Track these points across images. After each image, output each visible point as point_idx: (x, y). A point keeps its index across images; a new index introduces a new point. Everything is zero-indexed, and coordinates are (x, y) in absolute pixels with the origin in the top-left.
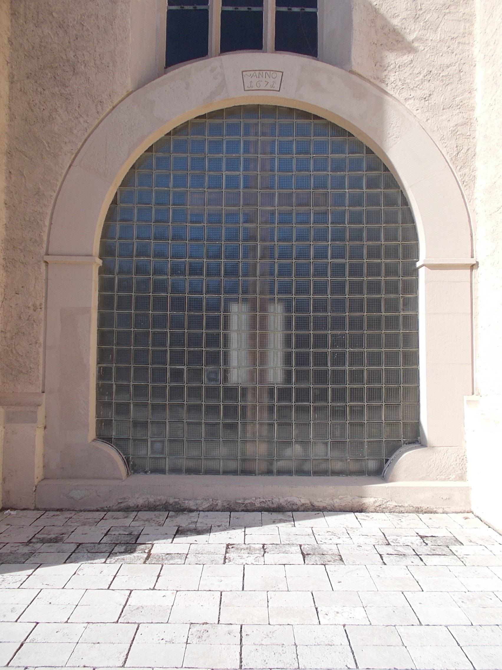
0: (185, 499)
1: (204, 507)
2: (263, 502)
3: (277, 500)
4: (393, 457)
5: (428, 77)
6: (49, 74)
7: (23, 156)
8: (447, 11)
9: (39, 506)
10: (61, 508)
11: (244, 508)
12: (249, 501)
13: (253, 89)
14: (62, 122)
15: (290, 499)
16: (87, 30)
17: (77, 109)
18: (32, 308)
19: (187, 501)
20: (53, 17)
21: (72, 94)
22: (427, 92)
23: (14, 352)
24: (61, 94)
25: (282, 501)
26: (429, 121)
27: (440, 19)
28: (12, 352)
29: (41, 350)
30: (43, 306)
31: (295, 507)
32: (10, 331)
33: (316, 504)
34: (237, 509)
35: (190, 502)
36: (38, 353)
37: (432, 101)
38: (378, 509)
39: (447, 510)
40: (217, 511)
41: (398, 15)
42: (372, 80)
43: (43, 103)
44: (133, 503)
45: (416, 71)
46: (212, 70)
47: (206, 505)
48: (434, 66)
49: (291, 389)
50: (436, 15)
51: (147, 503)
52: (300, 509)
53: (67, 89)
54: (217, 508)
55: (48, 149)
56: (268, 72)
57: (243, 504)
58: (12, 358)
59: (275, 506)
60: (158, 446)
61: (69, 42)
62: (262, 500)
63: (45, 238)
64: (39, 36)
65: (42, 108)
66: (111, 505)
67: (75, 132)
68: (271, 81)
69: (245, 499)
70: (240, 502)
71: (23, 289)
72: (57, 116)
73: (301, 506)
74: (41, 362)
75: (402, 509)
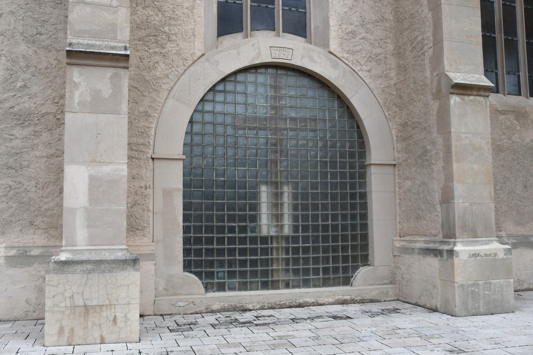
0: (246, 304)
1: (258, 307)
2: (291, 302)
3: (298, 301)
4: (356, 274)
5: (370, 59)
6: (153, 40)
7: (137, 90)
8: (378, 24)
9: (157, 313)
10: (171, 313)
11: (280, 307)
12: (283, 303)
13: (277, 58)
14: (161, 70)
15: (305, 300)
16: (177, 15)
17: (171, 63)
18: (144, 188)
19: (247, 305)
20: (155, 5)
21: (168, 53)
22: (369, 68)
23: (134, 216)
24: (161, 53)
25: (301, 301)
26: (51, 30)
27: (374, 28)
28: (132, 217)
29: (151, 214)
30: (151, 187)
31: (308, 304)
32: (130, 203)
33: (319, 302)
34: (276, 308)
35: (249, 305)
36: (149, 217)
37: (372, 73)
38: (352, 302)
39: (386, 300)
40: (265, 309)
41: (353, 24)
42: (341, 58)
43: (149, 58)
44: (216, 308)
45: (364, 55)
46: (253, 45)
47: (258, 307)
48: (372, 53)
49: (298, 237)
50: (372, 26)
51: (223, 307)
52: (311, 305)
53: (164, 50)
54: (265, 308)
55: (153, 87)
56: (285, 49)
57: (279, 304)
58: (132, 221)
59: (297, 304)
60: (220, 275)
61: (165, 21)
62: (290, 301)
63: (152, 143)
64: (146, 16)
65: (149, 60)
66: (202, 310)
67: (170, 77)
68: (286, 53)
69: (280, 302)
70: (278, 303)
71: (138, 175)
72: (158, 66)
73: (312, 303)
74: (151, 222)
75: (364, 301)
